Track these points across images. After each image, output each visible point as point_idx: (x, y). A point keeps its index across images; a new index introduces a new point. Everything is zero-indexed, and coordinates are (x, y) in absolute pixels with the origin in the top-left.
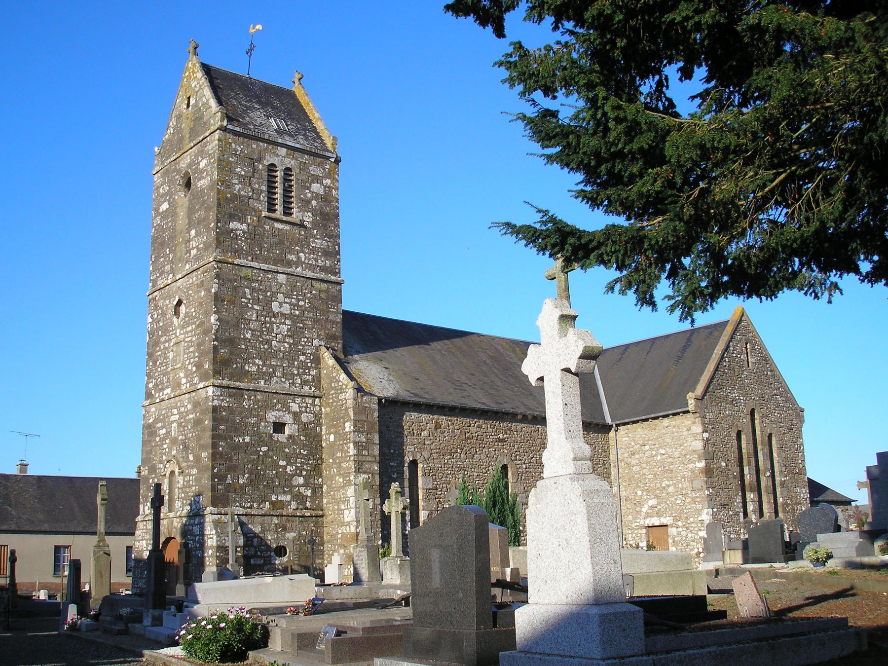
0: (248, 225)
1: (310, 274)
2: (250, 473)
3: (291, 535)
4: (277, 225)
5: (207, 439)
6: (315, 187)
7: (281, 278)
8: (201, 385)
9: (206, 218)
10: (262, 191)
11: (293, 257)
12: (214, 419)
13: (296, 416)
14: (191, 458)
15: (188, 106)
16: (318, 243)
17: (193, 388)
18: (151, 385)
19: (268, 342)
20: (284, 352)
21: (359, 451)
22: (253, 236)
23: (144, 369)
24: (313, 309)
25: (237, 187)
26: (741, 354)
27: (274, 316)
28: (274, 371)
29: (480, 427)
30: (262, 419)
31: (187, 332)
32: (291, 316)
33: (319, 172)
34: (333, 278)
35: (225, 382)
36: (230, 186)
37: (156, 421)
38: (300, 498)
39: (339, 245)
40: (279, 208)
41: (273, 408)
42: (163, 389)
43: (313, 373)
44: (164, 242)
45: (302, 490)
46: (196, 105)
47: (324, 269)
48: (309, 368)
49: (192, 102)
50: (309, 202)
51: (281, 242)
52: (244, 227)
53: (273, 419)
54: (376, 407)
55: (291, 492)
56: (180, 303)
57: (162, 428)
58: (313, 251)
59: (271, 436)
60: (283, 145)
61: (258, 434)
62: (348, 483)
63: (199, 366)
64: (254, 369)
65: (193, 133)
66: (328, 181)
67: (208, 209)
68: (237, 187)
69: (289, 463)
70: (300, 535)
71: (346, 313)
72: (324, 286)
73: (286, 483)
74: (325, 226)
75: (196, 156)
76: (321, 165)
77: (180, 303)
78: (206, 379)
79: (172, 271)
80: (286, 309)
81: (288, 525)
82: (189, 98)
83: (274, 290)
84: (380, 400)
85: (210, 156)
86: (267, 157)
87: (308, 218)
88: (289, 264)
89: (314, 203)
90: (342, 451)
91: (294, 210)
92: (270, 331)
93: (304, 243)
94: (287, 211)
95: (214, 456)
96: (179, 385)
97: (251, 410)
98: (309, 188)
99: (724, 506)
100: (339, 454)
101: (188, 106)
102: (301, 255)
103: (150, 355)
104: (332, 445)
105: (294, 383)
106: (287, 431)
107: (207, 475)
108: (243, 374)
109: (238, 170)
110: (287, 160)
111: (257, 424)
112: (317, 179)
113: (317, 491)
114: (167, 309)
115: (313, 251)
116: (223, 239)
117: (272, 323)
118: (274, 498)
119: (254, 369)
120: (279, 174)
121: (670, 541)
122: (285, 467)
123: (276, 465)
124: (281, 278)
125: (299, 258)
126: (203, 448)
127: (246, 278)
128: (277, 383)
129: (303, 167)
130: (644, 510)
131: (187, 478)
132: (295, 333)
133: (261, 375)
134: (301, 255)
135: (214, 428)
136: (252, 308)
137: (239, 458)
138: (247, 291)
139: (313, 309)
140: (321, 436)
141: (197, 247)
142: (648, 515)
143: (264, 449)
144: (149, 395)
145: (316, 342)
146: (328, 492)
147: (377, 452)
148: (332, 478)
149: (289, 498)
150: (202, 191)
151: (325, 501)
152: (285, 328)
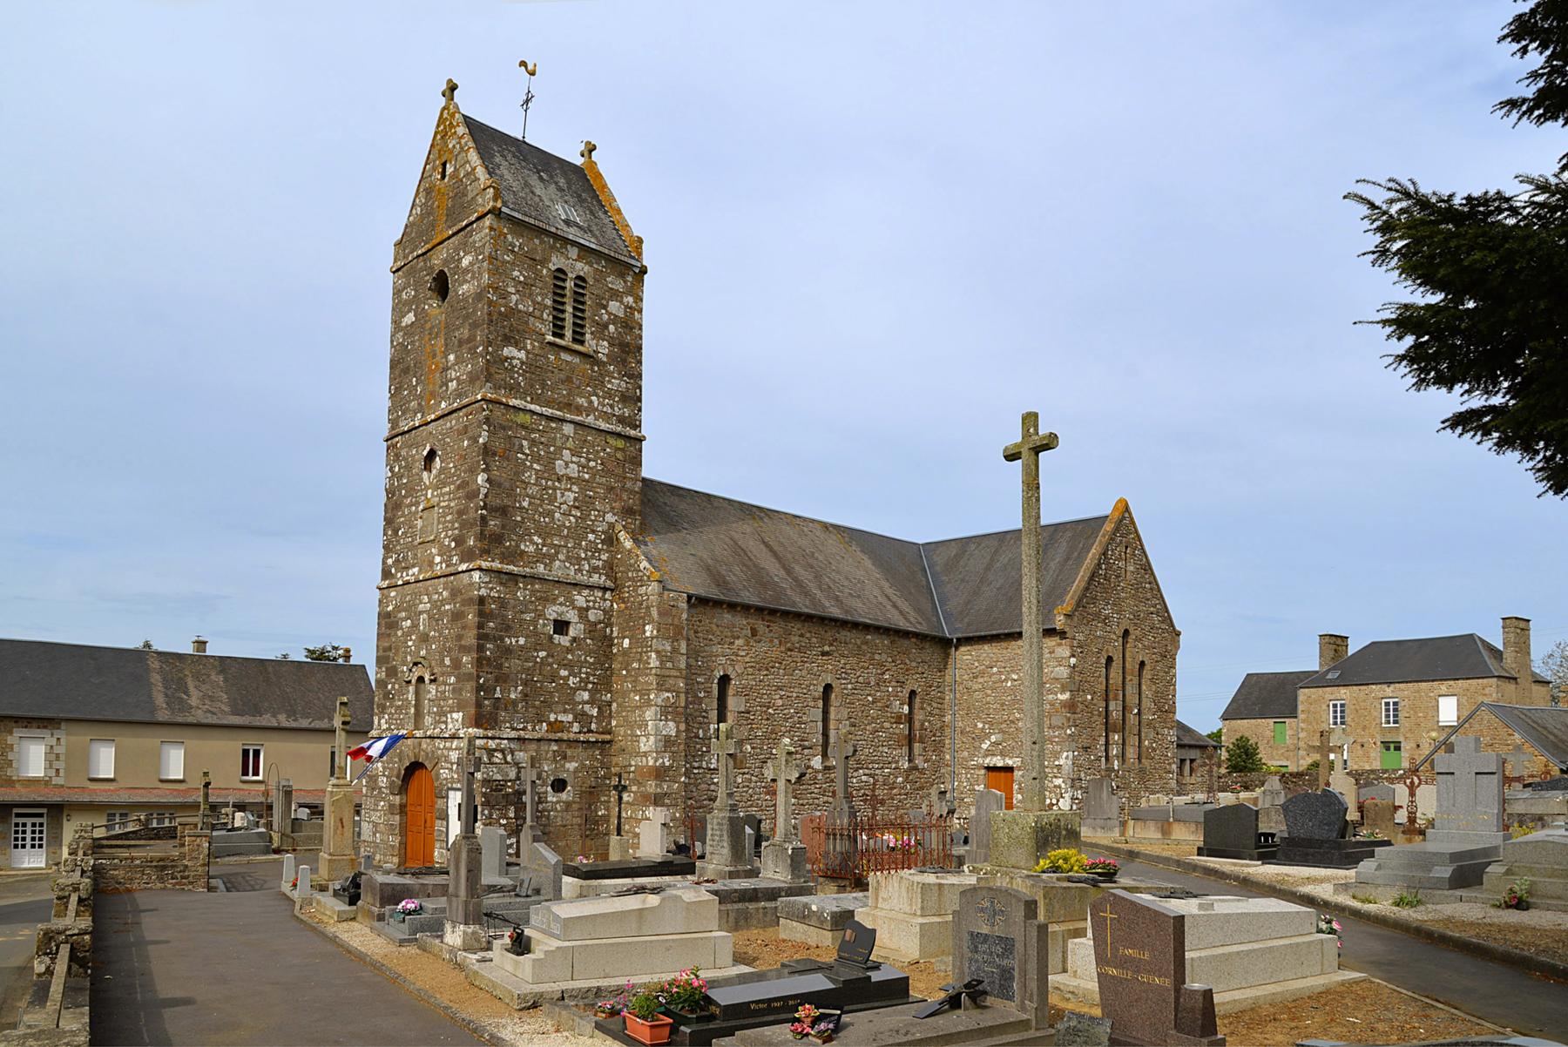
0: (528, 352)
1: (603, 425)
2: (525, 684)
3: (572, 766)
4: (565, 356)
5: (470, 639)
6: (614, 306)
7: (568, 429)
8: (464, 567)
9: (471, 339)
10: (546, 307)
11: (582, 401)
12: (481, 614)
13: (583, 612)
14: (447, 661)
15: (443, 177)
16: (615, 384)
17: (452, 570)
18: (390, 561)
19: (550, 514)
20: (569, 528)
21: (662, 662)
22: (531, 367)
23: (380, 540)
24: (606, 472)
25: (514, 298)
26: (1120, 559)
27: (559, 480)
28: (557, 553)
29: (802, 635)
30: (541, 615)
31: (443, 495)
32: (577, 480)
33: (619, 285)
34: (633, 433)
35: (497, 565)
36: (505, 296)
37: (398, 609)
38: (581, 717)
39: (640, 388)
40: (568, 333)
41: (554, 601)
42: (407, 568)
43: (604, 557)
44: (408, 368)
45: (587, 707)
46: (453, 176)
47: (621, 420)
48: (599, 551)
49: (450, 169)
50: (606, 326)
51: (569, 380)
52: (522, 355)
53: (554, 616)
54: (685, 606)
55: (572, 711)
56: (432, 455)
57: (406, 619)
58: (609, 394)
59: (551, 638)
60: (574, 243)
61: (536, 633)
62: (648, 703)
63: (459, 541)
64: (532, 548)
65: (452, 216)
66: (630, 299)
67: (475, 326)
68: (514, 298)
69: (572, 674)
70: (583, 766)
71: (644, 480)
72: (620, 443)
73: (569, 700)
74: (624, 361)
75: (457, 250)
76: (622, 276)
77: (432, 455)
78: (470, 560)
79: (421, 409)
80: (573, 470)
81: (569, 753)
82: (444, 165)
83: (559, 444)
84: (690, 597)
85: (478, 251)
86: (554, 259)
87: (604, 348)
88: (579, 410)
89: (612, 328)
90: (640, 661)
91: (588, 336)
92: (552, 499)
93: (598, 382)
94: (578, 338)
95: (480, 662)
96: (431, 564)
97: (525, 603)
98: (605, 307)
99: (1086, 749)
100: (635, 665)
101: (443, 177)
102: (594, 398)
103: (389, 521)
104: (625, 653)
105: (580, 570)
106: (572, 632)
107: (470, 685)
108: (514, 555)
109: (516, 273)
110: (579, 265)
111: (534, 622)
112: (616, 295)
113: (604, 708)
114: (414, 461)
115: (609, 394)
116: (493, 369)
117: (555, 489)
118: (552, 717)
119: (532, 548)
120: (569, 284)
121: (1016, 787)
122: (567, 678)
123: (554, 677)
124: (568, 429)
125: (591, 402)
126: (465, 650)
127: (523, 427)
128: (559, 569)
129: (600, 277)
130: (984, 746)
131: (442, 688)
132: (584, 504)
133: (540, 557)
134: (594, 398)
135: (480, 626)
136: (531, 467)
137: (512, 665)
138: (525, 443)
139: (606, 472)
140: (612, 639)
141: (458, 379)
142: (988, 753)
143: (543, 654)
144: (386, 574)
145: (610, 518)
146: (618, 712)
147: (683, 666)
148: (625, 694)
149: (570, 717)
150: (465, 300)
151: (614, 723)
152: (572, 496)
